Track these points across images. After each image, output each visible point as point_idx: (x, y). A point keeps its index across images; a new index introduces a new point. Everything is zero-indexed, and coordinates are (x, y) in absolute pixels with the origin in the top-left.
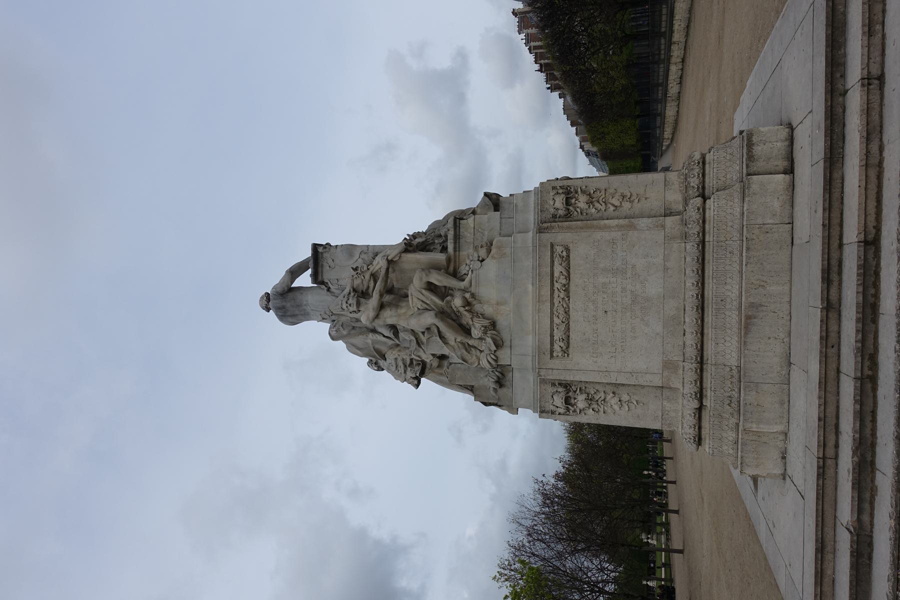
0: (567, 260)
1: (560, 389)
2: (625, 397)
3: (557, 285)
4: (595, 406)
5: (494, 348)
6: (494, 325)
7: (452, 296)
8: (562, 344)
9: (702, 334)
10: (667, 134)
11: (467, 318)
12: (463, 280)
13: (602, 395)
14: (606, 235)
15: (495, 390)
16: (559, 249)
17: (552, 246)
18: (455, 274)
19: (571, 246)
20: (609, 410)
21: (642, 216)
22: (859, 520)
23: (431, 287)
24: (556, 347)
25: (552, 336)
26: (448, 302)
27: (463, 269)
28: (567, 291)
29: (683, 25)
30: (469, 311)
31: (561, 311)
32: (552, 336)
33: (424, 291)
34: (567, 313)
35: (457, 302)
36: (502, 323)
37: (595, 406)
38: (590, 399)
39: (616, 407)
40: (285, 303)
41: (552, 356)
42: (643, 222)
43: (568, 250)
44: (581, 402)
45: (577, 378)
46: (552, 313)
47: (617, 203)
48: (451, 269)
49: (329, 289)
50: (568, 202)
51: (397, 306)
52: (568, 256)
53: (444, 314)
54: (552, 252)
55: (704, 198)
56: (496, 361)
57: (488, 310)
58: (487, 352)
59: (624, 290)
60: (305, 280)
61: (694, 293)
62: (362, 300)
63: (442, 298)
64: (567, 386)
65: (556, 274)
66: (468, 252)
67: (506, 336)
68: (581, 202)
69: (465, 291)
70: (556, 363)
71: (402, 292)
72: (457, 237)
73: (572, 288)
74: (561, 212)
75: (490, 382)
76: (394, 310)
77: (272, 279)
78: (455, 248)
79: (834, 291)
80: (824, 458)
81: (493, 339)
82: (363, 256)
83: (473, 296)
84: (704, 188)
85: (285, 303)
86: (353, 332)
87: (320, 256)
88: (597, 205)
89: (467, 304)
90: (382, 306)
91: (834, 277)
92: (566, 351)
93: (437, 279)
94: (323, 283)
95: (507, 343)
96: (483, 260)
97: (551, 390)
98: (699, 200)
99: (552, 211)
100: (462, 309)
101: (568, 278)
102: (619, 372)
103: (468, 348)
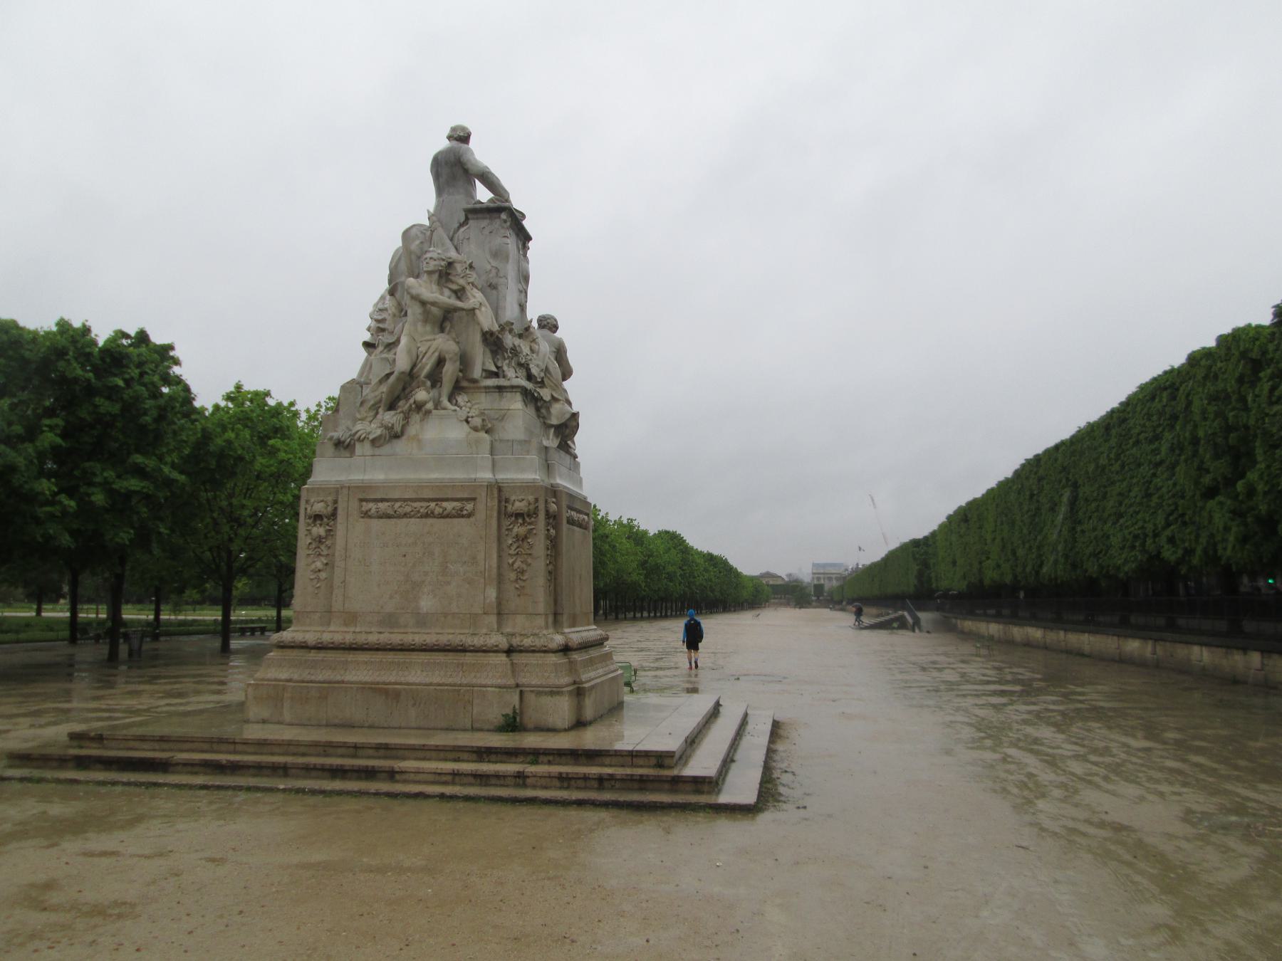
0: (459, 514)
1: (330, 509)
2: (323, 575)
3: (433, 505)
4: (313, 546)
5: (371, 437)
6: (397, 436)
7: (433, 386)
8: (373, 511)
9: (377, 649)
10: (968, 625)
11: (403, 405)
12: (450, 400)
13: (325, 553)
14: (481, 556)
15: (331, 438)
16: (469, 506)
17: (474, 499)
18: (457, 388)
19: (472, 519)
20: (310, 560)
21: (499, 591)
22: (177, 764)
23: (441, 362)
24: (371, 505)
25: (382, 500)
26: (424, 383)
27: (461, 399)
28: (427, 516)
29: (1087, 649)
30: (410, 409)
31: (408, 509)
32: (382, 500)
33: (436, 354)
34: (405, 515)
35: (421, 395)
36: (400, 446)
37: (313, 546)
38: (320, 540)
39: (313, 567)
40: (454, 169)
41: (361, 500)
42: (492, 593)
43: (469, 516)
44: (319, 530)
45: (339, 526)
46: (405, 500)
47: (516, 566)
48: (465, 384)
49: (461, 225)
50: (518, 515)
51: (426, 321)
52: (463, 516)
53: (410, 378)
54: (468, 500)
55: (510, 651)
56: (359, 439)
57: (412, 430)
58: (368, 429)
59: (426, 574)
60: (483, 194)
61: (428, 641)
62: (436, 276)
63: (429, 376)
64: (334, 515)
65: (445, 504)
66: (484, 402)
67: (386, 449)
68: (519, 530)
69: (437, 405)
70: (354, 504)
71: (448, 325)
72: (500, 389)
73: (430, 521)
74: (510, 508)
75: (339, 434)
76: (420, 317)
77: (481, 152)
78: (487, 388)
79: (371, 752)
80: (234, 743)
81: (380, 436)
82: (494, 271)
83: (429, 412)
84: (521, 651)
85: (454, 169)
86: (413, 257)
87: (495, 215)
88: (515, 546)
89: (419, 407)
90: (423, 303)
91: (382, 752)
92: (366, 515)
93: (450, 371)
94: (467, 219)
95: (377, 451)
96: (467, 422)
97: (330, 499)
98: (505, 645)
99: (513, 498)
100: (412, 401)
101: (441, 516)
102: (346, 569)
103: (375, 408)
